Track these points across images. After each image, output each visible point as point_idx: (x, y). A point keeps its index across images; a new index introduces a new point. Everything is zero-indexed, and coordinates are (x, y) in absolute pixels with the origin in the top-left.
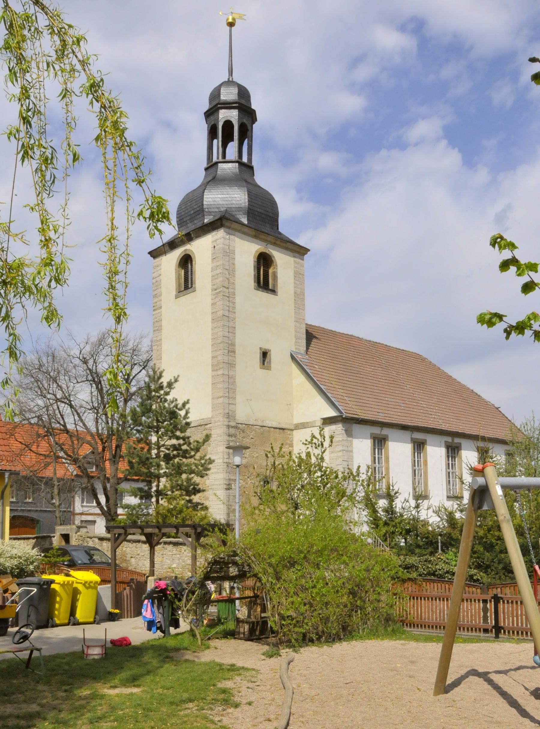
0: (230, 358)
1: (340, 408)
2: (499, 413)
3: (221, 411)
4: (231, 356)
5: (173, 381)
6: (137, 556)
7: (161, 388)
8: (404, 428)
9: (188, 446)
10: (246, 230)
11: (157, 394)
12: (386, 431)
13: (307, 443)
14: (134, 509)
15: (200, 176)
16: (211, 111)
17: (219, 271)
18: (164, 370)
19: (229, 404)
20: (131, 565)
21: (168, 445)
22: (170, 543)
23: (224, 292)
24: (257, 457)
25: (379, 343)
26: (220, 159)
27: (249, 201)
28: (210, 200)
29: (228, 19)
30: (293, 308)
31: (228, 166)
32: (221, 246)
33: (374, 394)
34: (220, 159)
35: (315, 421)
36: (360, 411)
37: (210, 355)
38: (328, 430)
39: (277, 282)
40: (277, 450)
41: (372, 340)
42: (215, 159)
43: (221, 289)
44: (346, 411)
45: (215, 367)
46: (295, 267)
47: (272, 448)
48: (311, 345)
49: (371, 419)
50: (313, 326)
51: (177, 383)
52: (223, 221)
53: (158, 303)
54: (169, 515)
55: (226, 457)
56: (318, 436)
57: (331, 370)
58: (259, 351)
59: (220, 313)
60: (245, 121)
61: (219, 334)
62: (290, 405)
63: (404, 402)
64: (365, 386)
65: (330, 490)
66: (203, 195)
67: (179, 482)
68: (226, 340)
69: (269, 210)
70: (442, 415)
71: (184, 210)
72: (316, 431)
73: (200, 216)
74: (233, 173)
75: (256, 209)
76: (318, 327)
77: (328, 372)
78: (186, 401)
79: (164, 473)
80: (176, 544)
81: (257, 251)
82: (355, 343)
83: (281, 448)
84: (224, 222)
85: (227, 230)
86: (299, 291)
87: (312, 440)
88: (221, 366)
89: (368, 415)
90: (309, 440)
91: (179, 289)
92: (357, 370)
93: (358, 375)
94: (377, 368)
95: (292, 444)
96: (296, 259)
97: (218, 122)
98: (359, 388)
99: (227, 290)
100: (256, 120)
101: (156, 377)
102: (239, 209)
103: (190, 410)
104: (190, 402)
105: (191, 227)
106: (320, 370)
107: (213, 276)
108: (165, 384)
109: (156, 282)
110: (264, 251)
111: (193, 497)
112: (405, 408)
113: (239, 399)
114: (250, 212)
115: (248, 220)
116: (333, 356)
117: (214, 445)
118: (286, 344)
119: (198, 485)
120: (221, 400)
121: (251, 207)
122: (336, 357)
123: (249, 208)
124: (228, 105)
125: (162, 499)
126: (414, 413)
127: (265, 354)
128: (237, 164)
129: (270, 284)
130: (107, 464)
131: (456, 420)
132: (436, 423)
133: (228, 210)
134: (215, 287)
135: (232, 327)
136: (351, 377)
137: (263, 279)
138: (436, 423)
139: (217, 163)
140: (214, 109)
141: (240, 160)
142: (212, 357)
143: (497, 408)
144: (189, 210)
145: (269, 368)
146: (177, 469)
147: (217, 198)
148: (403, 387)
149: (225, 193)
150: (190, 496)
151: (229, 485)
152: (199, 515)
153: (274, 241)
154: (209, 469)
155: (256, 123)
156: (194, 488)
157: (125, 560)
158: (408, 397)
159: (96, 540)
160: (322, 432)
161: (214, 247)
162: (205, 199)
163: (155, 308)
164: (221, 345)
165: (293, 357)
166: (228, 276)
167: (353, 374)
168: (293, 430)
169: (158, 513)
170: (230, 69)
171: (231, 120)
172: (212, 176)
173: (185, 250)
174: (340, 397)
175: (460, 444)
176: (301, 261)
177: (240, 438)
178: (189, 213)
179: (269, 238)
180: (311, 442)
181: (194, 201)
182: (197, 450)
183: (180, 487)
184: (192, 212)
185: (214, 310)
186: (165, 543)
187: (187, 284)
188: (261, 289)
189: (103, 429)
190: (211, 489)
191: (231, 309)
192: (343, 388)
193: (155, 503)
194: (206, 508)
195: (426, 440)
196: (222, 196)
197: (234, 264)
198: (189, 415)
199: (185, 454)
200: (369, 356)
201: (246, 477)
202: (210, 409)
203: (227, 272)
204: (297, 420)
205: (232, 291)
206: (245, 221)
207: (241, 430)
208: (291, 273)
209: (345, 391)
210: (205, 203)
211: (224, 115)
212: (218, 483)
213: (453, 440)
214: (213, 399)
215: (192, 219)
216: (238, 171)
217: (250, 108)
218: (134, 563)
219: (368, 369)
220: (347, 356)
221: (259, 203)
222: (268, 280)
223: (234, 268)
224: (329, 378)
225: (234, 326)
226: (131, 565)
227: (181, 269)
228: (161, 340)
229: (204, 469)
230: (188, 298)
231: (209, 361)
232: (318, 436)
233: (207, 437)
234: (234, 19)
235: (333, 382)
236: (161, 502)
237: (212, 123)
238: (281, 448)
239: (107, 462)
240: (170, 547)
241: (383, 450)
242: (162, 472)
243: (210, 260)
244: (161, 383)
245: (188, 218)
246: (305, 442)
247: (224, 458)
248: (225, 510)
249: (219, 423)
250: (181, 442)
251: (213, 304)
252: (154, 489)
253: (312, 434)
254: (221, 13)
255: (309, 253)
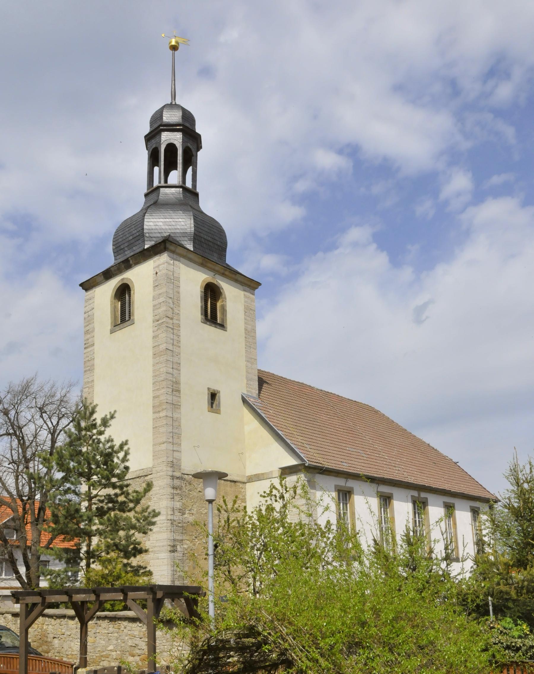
0: (175, 398)
1: (302, 455)
2: (458, 467)
3: (164, 459)
4: (175, 395)
5: (108, 417)
6: (61, 636)
7: (94, 426)
8: (372, 480)
9: (126, 497)
10: (192, 256)
11: (88, 433)
12: (351, 483)
13: (266, 495)
14: (59, 575)
15: (140, 202)
16: (153, 133)
17: (162, 299)
18: (97, 405)
19: (173, 451)
20: (53, 649)
21: (101, 496)
22: (105, 618)
23: (167, 323)
24: (206, 513)
25: (331, 393)
26: (163, 183)
27: (194, 226)
28: (151, 224)
29: (170, 43)
30: (244, 346)
31: (171, 191)
32: (165, 271)
33: (334, 442)
34: (163, 183)
35: (271, 472)
36: (323, 460)
37: (151, 395)
38: (291, 480)
39: (226, 316)
40: (230, 506)
41: (323, 389)
42: (156, 183)
43: (164, 320)
44: (308, 459)
45: (156, 409)
46: (245, 302)
47: (224, 501)
48: (263, 390)
49: (335, 468)
50: (262, 371)
51: (113, 420)
52: (165, 245)
53: (89, 340)
54: (103, 581)
55: (170, 512)
56: (278, 486)
57: (286, 415)
58: (206, 392)
59: (163, 347)
60: (189, 145)
61: (161, 370)
62: (242, 453)
63: (365, 452)
64: (323, 434)
65: (296, 547)
66: (144, 219)
67: (117, 541)
68: (170, 377)
69: (217, 238)
70: (406, 468)
71: (121, 236)
72: (276, 482)
73: (140, 241)
74: (176, 198)
75: (202, 235)
76: (267, 373)
77: (284, 418)
78: (124, 441)
79: (96, 530)
80: (113, 619)
81: (204, 281)
82: (307, 391)
83: (235, 502)
84: (168, 245)
85: (171, 254)
86: (249, 327)
87: (271, 492)
88: (164, 407)
89: (331, 464)
90: (268, 492)
91: (115, 323)
92: (314, 417)
93: (315, 423)
94: (332, 417)
95: (245, 499)
96: (246, 293)
97: (160, 145)
98: (318, 436)
99: (171, 321)
100: (201, 148)
101: (88, 412)
102: (184, 234)
103: (130, 451)
104: (129, 442)
105: (129, 253)
106: (274, 415)
107: (154, 306)
108: (99, 422)
109: (89, 316)
110: (212, 281)
111: (132, 559)
112: (368, 459)
113: (185, 445)
114: (196, 238)
115: (194, 247)
116: (287, 402)
117: (155, 499)
118: (235, 388)
119: (139, 544)
120: (164, 447)
121: (197, 233)
122: (290, 403)
123: (195, 234)
124: (171, 128)
125: (93, 562)
126: (377, 464)
127: (213, 396)
128: (181, 189)
129: (218, 318)
130: (28, 527)
131: (420, 474)
132: (401, 475)
133: (172, 235)
134: (157, 317)
135: (177, 363)
136: (308, 424)
137: (211, 312)
138: (401, 475)
139: (158, 188)
140: (157, 130)
141: (183, 185)
142: (154, 397)
143: (456, 463)
144: (128, 236)
145: (218, 411)
146: (113, 525)
147: (158, 224)
148: (363, 438)
149: (168, 217)
150: (128, 558)
151: (174, 546)
152: (141, 581)
153: (222, 271)
154: (154, 524)
155: (201, 150)
156: (135, 548)
157: (46, 642)
158: (369, 448)
159: (9, 616)
160: (283, 482)
161: (157, 273)
162: (145, 223)
163: (86, 346)
164: (164, 383)
165: (244, 401)
166: (172, 306)
167: (309, 422)
168: (244, 483)
169: (88, 579)
170: (173, 93)
171: (175, 143)
172: (153, 199)
173: (123, 279)
174: (299, 444)
175: (427, 498)
176: (251, 296)
177: (187, 491)
178: (127, 240)
179: (218, 268)
180: (270, 494)
181: (133, 226)
182: (137, 501)
183: (117, 547)
184: (131, 238)
185: (156, 344)
186: (99, 618)
187: (124, 316)
188: (208, 323)
189: (23, 485)
190: (152, 551)
191: (175, 343)
192: (302, 435)
193: (84, 567)
194: (150, 573)
195: (392, 494)
196: (165, 220)
197: (179, 293)
198: (128, 457)
199: (123, 507)
200: (323, 405)
201: (194, 537)
202: (151, 457)
203: (170, 301)
204: (250, 471)
205: (177, 322)
206: (191, 247)
207: (187, 481)
208: (241, 308)
209: (305, 439)
210: (145, 227)
211: (166, 137)
212: (161, 544)
213: (419, 495)
214: (154, 445)
215: (130, 246)
216: (182, 196)
217: (195, 132)
218: (57, 646)
219: (324, 418)
220: (301, 403)
221: (206, 230)
222: (216, 314)
223: (179, 297)
224: (286, 424)
225: (179, 362)
226: (53, 649)
227: (117, 300)
228: (93, 381)
229: (147, 523)
230: (125, 332)
231: (150, 403)
232: (278, 486)
233: (149, 486)
234: (177, 42)
235: (290, 429)
236: (92, 566)
237: (154, 146)
238: (235, 502)
239: (28, 525)
240: (105, 623)
241: (348, 505)
242: (94, 528)
243: (151, 288)
244: (94, 420)
245: (126, 245)
246: (263, 494)
247: (167, 514)
248: (170, 577)
249: (161, 474)
250: (118, 491)
251: (154, 337)
252: (84, 549)
253: (272, 484)
254: (163, 35)
255: (260, 287)
